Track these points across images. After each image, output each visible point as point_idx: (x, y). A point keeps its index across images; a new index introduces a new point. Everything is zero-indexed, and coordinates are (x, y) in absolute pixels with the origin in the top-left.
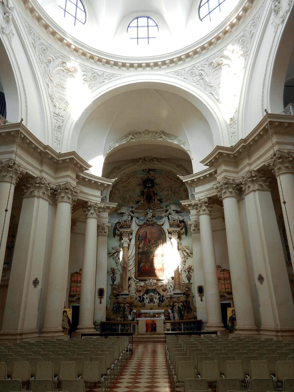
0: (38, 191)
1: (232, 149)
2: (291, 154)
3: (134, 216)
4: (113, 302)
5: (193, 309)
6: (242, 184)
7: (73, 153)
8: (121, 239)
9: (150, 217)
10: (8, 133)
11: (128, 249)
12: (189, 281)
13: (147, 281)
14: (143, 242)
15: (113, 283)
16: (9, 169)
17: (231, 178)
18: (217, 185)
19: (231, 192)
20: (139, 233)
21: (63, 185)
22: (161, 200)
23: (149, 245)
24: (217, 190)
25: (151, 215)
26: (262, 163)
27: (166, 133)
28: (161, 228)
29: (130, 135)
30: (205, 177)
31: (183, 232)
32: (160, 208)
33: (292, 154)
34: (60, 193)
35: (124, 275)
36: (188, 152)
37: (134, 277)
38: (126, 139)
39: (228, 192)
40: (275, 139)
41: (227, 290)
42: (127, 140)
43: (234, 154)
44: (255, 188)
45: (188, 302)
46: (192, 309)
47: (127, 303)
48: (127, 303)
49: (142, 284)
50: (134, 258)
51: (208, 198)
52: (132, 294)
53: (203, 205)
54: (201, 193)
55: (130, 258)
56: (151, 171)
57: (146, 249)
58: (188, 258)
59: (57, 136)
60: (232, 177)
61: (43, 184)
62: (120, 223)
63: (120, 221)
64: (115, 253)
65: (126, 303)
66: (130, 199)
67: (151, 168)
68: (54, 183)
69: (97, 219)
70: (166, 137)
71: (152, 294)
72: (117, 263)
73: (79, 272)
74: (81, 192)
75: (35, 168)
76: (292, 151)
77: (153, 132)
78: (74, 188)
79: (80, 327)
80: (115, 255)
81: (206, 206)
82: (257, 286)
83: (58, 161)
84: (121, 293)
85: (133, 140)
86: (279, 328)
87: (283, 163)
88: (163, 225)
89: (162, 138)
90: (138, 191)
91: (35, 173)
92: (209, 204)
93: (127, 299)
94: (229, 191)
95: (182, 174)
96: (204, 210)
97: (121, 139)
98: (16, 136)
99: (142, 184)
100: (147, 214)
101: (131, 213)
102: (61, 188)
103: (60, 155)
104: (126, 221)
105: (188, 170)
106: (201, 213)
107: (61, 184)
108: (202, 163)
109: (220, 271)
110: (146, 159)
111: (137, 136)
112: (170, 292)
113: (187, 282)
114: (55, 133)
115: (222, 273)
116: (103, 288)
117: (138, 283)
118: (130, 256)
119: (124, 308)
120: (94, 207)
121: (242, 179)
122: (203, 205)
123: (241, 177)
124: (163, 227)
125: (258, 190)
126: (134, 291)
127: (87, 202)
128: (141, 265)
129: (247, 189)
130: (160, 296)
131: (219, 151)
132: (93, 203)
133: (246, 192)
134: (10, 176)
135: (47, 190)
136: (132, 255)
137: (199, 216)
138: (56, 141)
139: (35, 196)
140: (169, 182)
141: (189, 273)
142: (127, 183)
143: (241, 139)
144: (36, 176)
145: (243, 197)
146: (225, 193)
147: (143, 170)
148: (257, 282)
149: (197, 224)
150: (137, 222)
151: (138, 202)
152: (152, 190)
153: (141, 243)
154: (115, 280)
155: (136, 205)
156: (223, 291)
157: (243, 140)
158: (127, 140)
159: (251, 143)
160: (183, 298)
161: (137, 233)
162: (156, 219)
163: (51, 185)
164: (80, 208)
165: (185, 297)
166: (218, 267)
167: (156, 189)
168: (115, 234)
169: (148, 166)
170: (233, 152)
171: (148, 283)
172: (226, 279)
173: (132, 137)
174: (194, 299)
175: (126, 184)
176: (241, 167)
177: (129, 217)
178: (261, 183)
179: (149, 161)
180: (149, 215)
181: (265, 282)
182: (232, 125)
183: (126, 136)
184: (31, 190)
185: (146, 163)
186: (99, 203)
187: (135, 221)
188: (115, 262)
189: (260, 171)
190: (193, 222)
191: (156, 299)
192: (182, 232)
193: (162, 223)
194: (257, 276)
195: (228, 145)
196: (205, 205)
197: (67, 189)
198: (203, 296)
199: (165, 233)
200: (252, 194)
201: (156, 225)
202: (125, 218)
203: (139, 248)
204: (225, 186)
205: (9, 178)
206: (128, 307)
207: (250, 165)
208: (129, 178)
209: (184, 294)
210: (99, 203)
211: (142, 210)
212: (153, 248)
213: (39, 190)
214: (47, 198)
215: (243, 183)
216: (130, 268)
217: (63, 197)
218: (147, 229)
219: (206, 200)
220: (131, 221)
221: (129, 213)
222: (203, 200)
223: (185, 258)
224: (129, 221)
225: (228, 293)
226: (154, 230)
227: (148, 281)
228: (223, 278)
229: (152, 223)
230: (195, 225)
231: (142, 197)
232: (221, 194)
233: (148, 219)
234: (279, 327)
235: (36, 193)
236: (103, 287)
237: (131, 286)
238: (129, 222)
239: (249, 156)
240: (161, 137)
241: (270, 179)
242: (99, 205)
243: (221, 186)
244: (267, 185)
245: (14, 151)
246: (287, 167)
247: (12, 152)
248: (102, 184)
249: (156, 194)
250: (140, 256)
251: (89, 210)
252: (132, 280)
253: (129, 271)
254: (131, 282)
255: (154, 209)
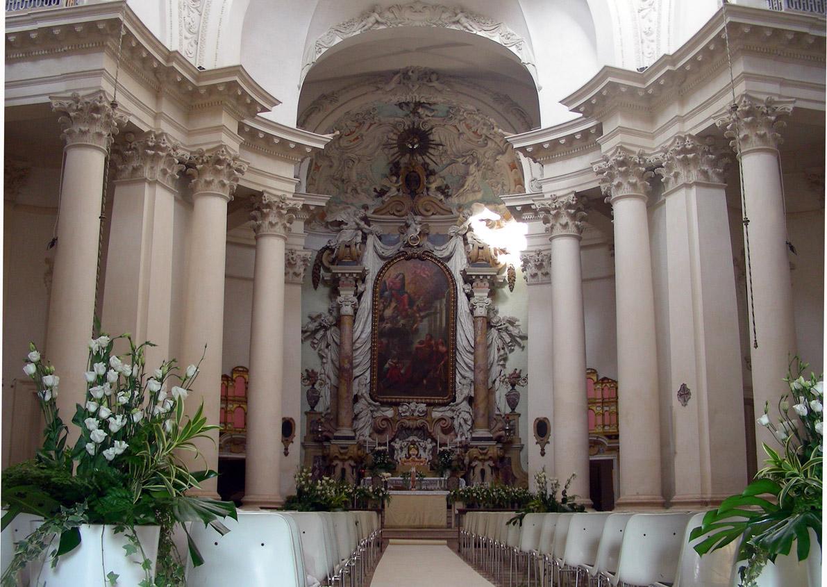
0: (152, 168)
1: (643, 74)
2: (774, 106)
3: (371, 233)
4: (312, 457)
5: (518, 477)
6: (662, 167)
7: (237, 70)
8: (335, 292)
9: (415, 235)
10: (91, 26)
11: (354, 321)
12: (513, 409)
13: (403, 405)
14: (393, 305)
15: (312, 408)
16: (95, 115)
17: (637, 150)
18: (601, 164)
19: (634, 185)
20: (383, 279)
21: (208, 151)
22: (446, 191)
23: (410, 311)
24: (600, 176)
25: (419, 230)
26: (709, 118)
27: (472, 13)
28: (445, 267)
29: (374, 12)
30: (571, 138)
31: (504, 280)
32: (442, 211)
33: (777, 106)
34: (200, 173)
35: (343, 389)
36: (530, 68)
37: (367, 396)
38: (364, 23)
39: (625, 185)
40: (739, 68)
41: (606, 428)
42: (366, 27)
43: (646, 90)
44: (690, 179)
45: (506, 461)
46: (515, 478)
47: (350, 458)
48: (350, 458)
49: (389, 413)
50: (369, 346)
51: (577, 194)
52: (361, 438)
53: (563, 211)
54: (561, 179)
55: (357, 345)
56: (422, 107)
57: (402, 321)
58: (513, 350)
59: (191, 23)
60: (639, 146)
61: (162, 149)
62: (333, 251)
63: (332, 244)
64: (316, 331)
65: (346, 457)
66: (361, 183)
67: (423, 100)
68: (186, 146)
69: (286, 239)
70: (471, 23)
71: (416, 439)
72: (322, 357)
73: (229, 375)
74: (252, 170)
75: (144, 109)
76: (776, 99)
77: (435, 7)
78: (235, 159)
79: (250, 500)
80: (319, 336)
81: (569, 214)
82: (673, 411)
83: (196, 89)
84: (335, 434)
85: (381, 27)
86: (708, 496)
87: (754, 127)
88: (449, 258)
89: (461, 24)
90: (381, 164)
91: (144, 122)
92: (579, 210)
93: (351, 448)
94: (629, 183)
95: (514, 128)
96: (565, 226)
97: (350, 23)
98: (109, 32)
99: (395, 142)
100: (408, 226)
101: (362, 223)
102: (203, 160)
103: (201, 73)
104: (349, 246)
105: (528, 115)
106: (556, 233)
107: (204, 148)
108: (565, 104)
109: (595, 383)
110: (410, 73)
111: (391, 16)
112: (463, 434)
113: (508, 410)
114: (185, 13)
115: (598, 386)
116: (291, 419)
117: (376, 411)
118: (359, 341)
119: (343, 470)
120: (278, 207)
121: (663, 154)
122: (563, 211)
123: (659, 149)
124: (449, 264)
125: (697, 184)
126: (367, 432)
127: (261, 194)
128: (387, 366)
129: (673, 179)
130: (437, 443)
131: (610, 79)
132: (275, 195)
133: (670, 187)
134: (97, 133)
135: (171, 163)
136: (364, 336)
137: (551, 240)
138: (189, 36)
139: (145, 180)
140: (470, 140)
141: (513, 389)
142: (354, 140)
143: (665, 55)
144: (146, 129)
145: (663, 198)
146: (619, 186)
147: (400, 104)
148: (676, 402)
149: (542, 261)
150: (378, 248)
151: (381, 193)
152: (422, 161)
153: (389, 305)
154: (316, 402)
155: (376, 200)
156: (597, 431)
157: (670, 58)
158: (366, 27)
159: (688, 68)
160: (495, 450)
161: (378, 280)
162: (433, 242)
163: (180, 152)
164: (246, 208)
165: (501, 448)
166: (590, 372)
167: (434, 159)
168: (316, 280)
169: (415, 94)
170: (644, 83)
171: (404, 412)
172: (606, 402)
173: (380, 20)
174: (522, 454)
175: (351, 142)
176: (662, 122)
177: (356, 235)
178: (705, 168)
179: (418, 79)
180: (411, 229)
181: (692, 402)
182: (646, 11)
183: (364, 16)
184: (135, 164)
185: (411, 86)
186: (290, 196)
187: (374, 246)
188: (317, 355)
189: (705, 137)
190: (533, 254)
191: (425, 451)
192: (502, 281)
193: (446, 254)
194: (676, 388)
195: (633, 67)
196: (568, 212)
197: (219, 162)
198: (548, 442)
199: (454, 281)
200: (683, 191)
201: (432, 257)
202: (347, 235)
203: (382, 319)
204: (620, 169)
205: (93, 136)
206: (353, 467)
207: (681, 119)
208: (360, 124)
209: (499, 440)
210: (290, 196)
211: (394, 214)
212: (421, 321)
213: (153, 165)
214: (170, 185)
215: (663, 165)
216: (357, 372)
217: (209, 183)
218: (406, 269)
219: (571, 199)
220: (363, 246)
221: (357, 224)
222: (562, 199)
223: (506, 349)
224: (356, 245)
225: (609, 437)
226: (425, 271)
227: (405, 407)
228: (600, 401)
229: (420, 251)
230: (538, 263)
231: (394, 178)
232: (609, 189)
233: (408, 242)
234: (709, 496)
235: (147, 173)
236: (290, 416)
237: (359, 417)
238: (358, 247)
239: (683, 98)
240: (458, 22)
241: (726, 160)
242: (291, 204)
243: (611, 167)
244: (718, 174)
245: (104, 69)
246: (762, 137)
247: (100, 72)
248: (299, 146)
249: (432, 173)
250: (384, 341)
251: (264, 216)
252: (363, 401)
253: (355, 378)
254: (361, 405)
255: (425, 213)
